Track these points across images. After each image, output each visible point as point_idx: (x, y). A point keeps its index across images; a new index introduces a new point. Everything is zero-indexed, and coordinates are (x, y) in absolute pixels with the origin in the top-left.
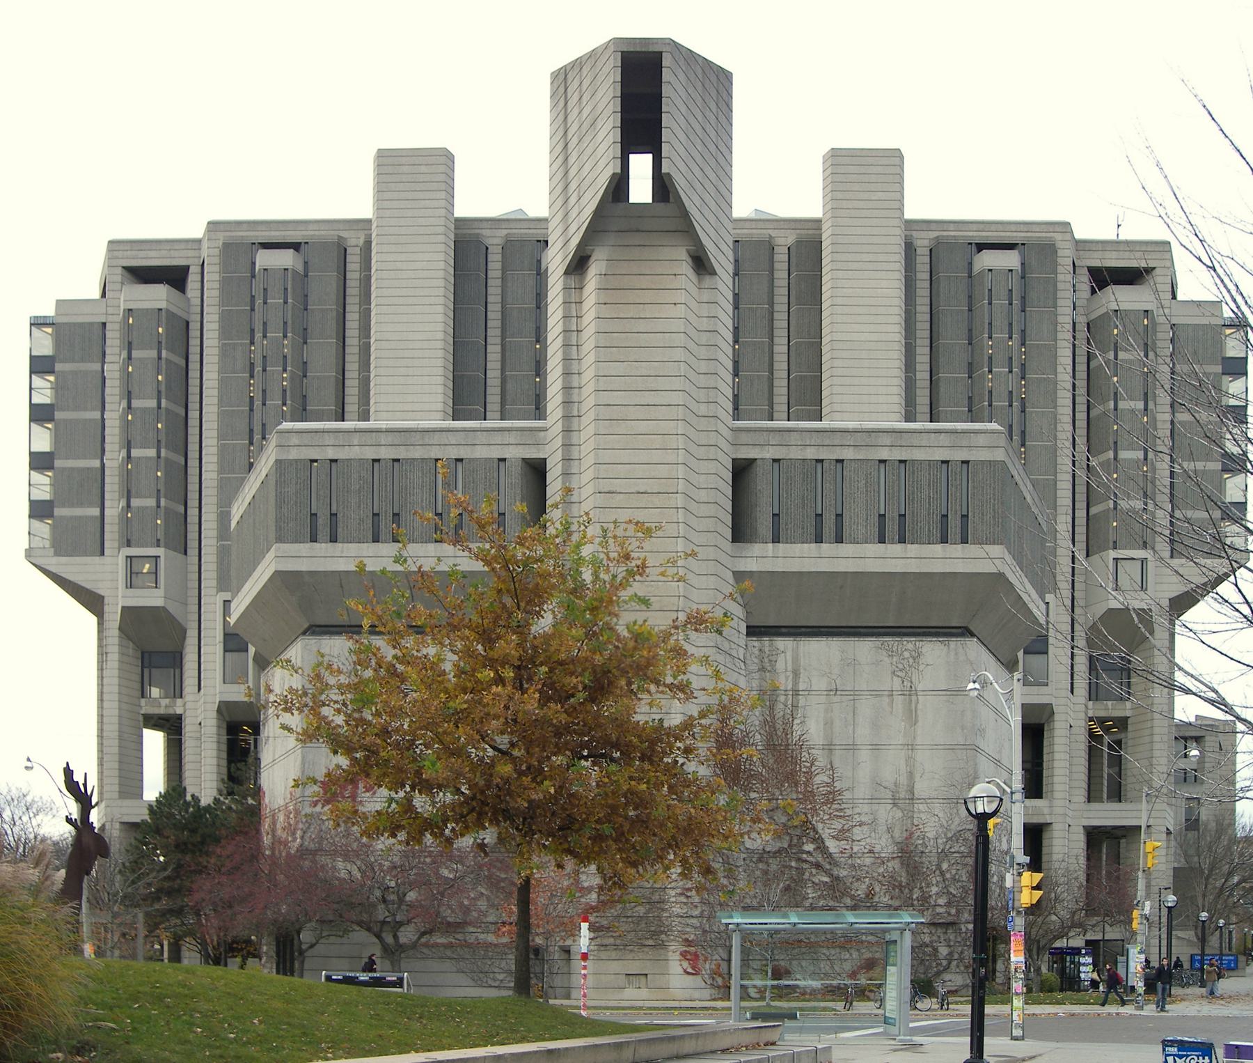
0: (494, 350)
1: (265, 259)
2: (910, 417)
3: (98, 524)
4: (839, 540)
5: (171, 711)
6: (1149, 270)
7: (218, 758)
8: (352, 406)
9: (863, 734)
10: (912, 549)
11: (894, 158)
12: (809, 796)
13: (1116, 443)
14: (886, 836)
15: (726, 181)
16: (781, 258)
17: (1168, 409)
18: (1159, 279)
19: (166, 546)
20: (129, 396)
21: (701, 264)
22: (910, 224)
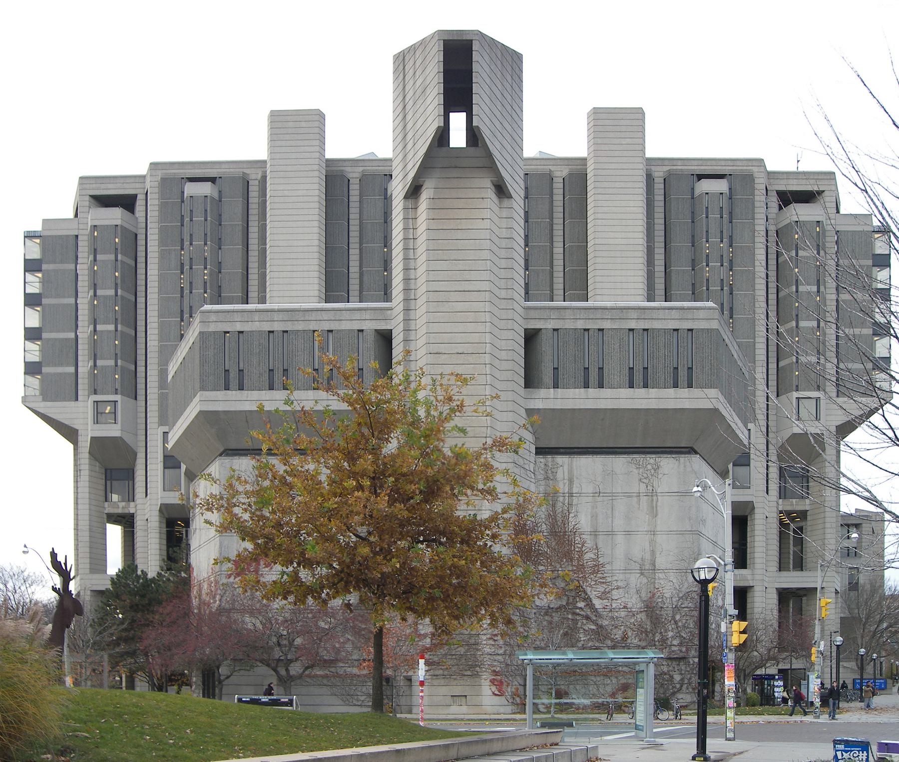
0: (354, 253)
1: (191, 189)
4: (601, 386)
5: (126, 511)
6: (820, 193)
9: (619, 523)
10: (653, 392)
11: (639, 113)
12: (581, 568)
13: (797, 316)
14: (636, 596)
16: (558, 186)
17: (834, 291)
18: (827, 199)
19: (122, 394)
20: (95, 287)
21: (501, 190)
22: (650, 161)
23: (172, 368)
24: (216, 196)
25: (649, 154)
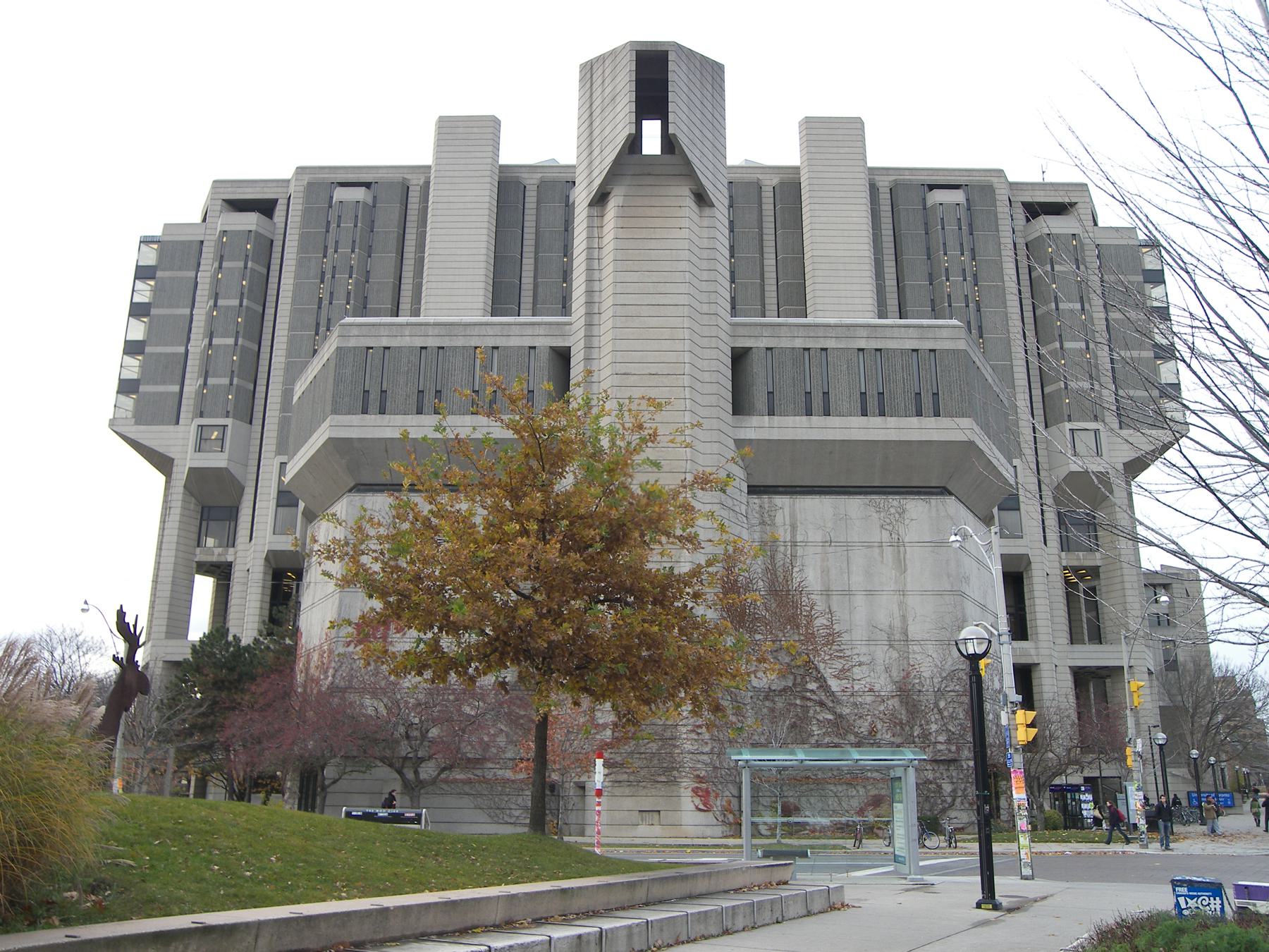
0: (528, 263)
1: (340, 194)
4: (827, 413)
5: (223, 559)
6: (1073, 205)
10: (892, 421)
15: (721, 140)
16: (768, 195)
21: (702, 199)
22: (873, 171)
23: (299, 388)
24: (370, 201)
25: (872, 162)
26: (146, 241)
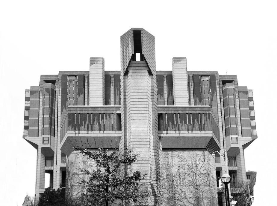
1: (69, 78)
2: (190, 104)
3: (38, 130)
5: (51, 169)
7: (60, 177)
8: (86, 103)
15: (154, 55)
20: (44, 105)
21: (150, 73)
26: (27, 91)
